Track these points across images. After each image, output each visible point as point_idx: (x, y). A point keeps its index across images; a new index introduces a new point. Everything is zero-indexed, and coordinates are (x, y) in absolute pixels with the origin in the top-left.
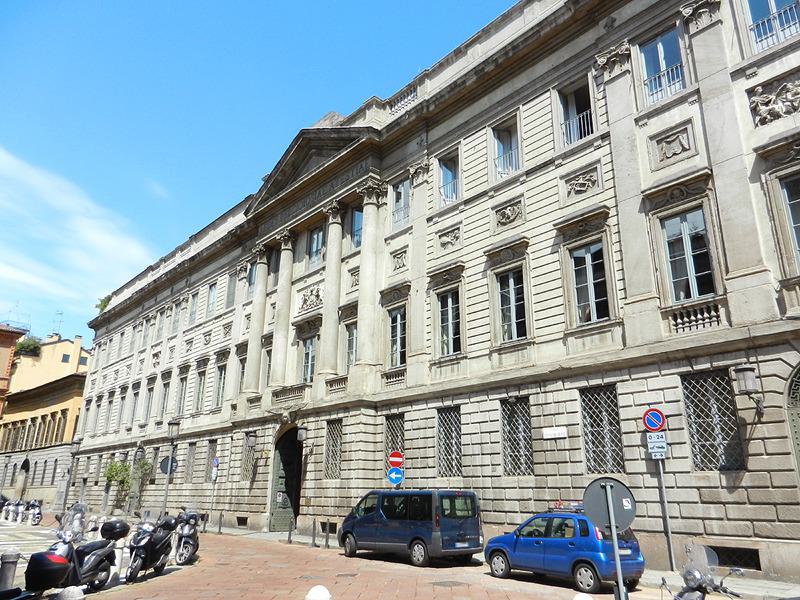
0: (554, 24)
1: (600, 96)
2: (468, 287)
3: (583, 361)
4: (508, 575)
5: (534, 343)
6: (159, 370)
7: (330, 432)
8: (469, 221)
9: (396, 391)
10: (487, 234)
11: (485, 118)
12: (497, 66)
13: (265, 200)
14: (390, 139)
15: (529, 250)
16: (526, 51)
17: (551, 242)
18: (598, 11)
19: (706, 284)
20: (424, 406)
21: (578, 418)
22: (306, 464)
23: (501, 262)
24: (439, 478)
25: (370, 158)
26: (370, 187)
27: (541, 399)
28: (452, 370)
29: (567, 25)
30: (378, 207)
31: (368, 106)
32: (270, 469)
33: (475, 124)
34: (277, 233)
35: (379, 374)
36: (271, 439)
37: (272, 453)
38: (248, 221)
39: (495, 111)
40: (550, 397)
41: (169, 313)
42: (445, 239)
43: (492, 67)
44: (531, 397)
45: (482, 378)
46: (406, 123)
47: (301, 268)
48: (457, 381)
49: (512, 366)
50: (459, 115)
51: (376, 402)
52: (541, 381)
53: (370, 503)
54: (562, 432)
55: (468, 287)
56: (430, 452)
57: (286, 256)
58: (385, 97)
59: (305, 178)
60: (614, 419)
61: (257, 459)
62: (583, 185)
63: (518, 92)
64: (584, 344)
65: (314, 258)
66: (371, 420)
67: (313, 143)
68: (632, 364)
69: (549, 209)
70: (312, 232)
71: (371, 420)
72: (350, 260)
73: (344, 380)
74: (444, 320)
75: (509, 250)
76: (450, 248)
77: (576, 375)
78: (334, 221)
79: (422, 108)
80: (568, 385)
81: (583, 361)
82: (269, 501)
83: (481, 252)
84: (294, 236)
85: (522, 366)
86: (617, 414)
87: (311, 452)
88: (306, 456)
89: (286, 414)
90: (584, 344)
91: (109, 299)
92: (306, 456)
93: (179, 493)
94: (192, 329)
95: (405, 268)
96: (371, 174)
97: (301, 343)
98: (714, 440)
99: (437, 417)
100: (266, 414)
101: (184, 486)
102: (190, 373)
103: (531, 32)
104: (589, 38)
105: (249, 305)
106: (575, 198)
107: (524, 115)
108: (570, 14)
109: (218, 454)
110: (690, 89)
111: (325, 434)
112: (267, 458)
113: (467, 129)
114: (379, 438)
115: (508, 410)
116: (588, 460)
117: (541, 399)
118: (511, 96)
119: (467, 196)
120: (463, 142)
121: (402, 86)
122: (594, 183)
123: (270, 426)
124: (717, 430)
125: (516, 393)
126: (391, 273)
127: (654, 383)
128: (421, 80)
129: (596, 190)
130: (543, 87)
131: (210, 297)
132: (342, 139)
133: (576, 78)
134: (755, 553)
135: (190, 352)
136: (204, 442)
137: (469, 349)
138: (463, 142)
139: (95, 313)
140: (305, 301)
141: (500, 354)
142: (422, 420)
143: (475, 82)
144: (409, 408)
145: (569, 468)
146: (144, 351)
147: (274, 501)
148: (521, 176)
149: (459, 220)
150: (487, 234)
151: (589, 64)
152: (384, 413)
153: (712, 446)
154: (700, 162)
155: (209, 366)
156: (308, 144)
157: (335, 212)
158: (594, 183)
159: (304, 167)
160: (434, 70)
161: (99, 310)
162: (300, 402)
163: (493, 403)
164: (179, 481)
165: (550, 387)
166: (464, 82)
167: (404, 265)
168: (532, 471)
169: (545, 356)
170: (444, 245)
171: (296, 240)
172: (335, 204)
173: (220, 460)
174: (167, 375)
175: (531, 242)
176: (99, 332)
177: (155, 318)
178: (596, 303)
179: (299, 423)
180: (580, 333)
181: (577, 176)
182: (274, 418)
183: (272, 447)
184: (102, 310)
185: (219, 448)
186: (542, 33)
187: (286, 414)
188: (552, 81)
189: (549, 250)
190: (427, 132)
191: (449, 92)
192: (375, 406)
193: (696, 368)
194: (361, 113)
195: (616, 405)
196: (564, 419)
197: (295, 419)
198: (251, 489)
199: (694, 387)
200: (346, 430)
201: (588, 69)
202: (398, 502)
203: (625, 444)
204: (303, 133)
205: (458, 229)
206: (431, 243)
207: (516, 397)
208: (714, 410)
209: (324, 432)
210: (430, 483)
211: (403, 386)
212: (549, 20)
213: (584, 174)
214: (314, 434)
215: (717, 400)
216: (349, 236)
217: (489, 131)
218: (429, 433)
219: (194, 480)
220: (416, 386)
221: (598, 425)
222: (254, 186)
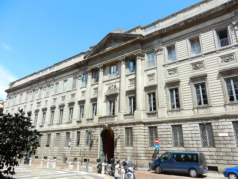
0: (216, 11)
1: (233, 33)
2: (182, 88)
3: (234, 113)
4: (160, 173)
5: (212, 106)
6: (40, 108)
7: (126, 132)
8: (207, 60)
9: (153, 119)
10: (189, 72)
11: (187, 35)
12: (193, 21)
13: (92, 55)
14: (147, 39)
15: (207, 78)
16: (203, 17)
17: (188, 82)
18: (232, 8)
19: (155, 109)
20: (166, 124)
21: (232, 130)
22: (116, 142)
23: (196, 81)
24: (174, 148)
25: (139, 44)
26: (140, 54)
27: (217, 124)
28: (177, 113)
29: (220, 11)
30: (142, 60)
31: (137, 28)
32: (99, 143)
33: (182, 37)
34: (98, 65)
35: (145, 114)
36: (99, 133)
37: (100, 138)
38: (84, 61)
39: (190, 34)
40: (220, 124)
41: (45, 89)
42: (170, 72)
43: (191, 21)
44: (158, 127)
45: (192, 116)
46: (155, 35)
47: (107, 77)
48: (180, 117)
49: (176, 116)
50: (176, 34)
51: (145, 122)
52: (217, 118)
53: (167, 156)
54: (227, 135)
55: (182, 88)
56: (170, 139)
57: (101, 73)
58: (142, 26)
59: (108, 49)
60: (156, 134)
61: (93, 139)
62: (228, 60)
63: (200, 29)
64: (233, 108)
65: (112, 74)
66: (143, 128)
67: (113, 38)
68: (187, 120)
69: (187, 72)
70: (111, 66)
71: (143, 128)
72: (129, 76)
73: (43, 126)
74: (110, 108)
75: (200, 77)
76: (173, 75)
77: (230, 117)
78: (124, 63)
79: (162, 31)
80: (227, 120)
81: (234, 113)
82: (99, 154)
83: (218, 71)
84: (104, 67)
85: (208, 113)
86: (157, 133)
87: (119, 138)
88: (116, 139)
89: (107, 125)
90: (233, 108)
91: (14, 82)
92: (116, 139)
93: (52, 150)
94: (14, 106)
95: (154, 80)
96: (140, 49)
97: (108, 102)
98: (178, 140)
99: (148, 129)
100: (97, 125)
101: (55, 148)
102: (56, 109)
103: (208, 12)
104: (228, 16)
105: (83, 88)
106: (224, 63)
107: (177, 45)
108: (223, 8)
109: (71, 137)
110: (156, 67)
111: (124, 132)
112: (98, 139)
113: (179, 39)
114: (146, 134)
115: (202, 127)
116: (125, 144)
117: (217, 124)
118: (197, 30)
119: (205, 52)
120: (177, 43)
121: (150, 23)
122: (232, 59)
123: (98, 128)
124: (208, 137)
125: (206, 122)
126: (147, 81)
127: (192, 125)
128: (158, 22)
129: (233, 61)
130: (210, 29)
131: (65, 85)
132: (127, 37)
133: (222, 28)
134: (217, 167)
135: (55, 103)
136: (64, 134)
137: (212, 103)
138: (177, 43)
139: (8, 88)
140: (109, 88)
141: (197, 109)
142: (165, 130)
143: (183, 25)
144: (159, 125)
145: (230, 146)
146: (33, 101)
147: (100, 154)
148: (203, 55)
149: (177, 67)
150: (189, 72)
151: (228, 24)
152: (148, 126)
153: (177, 142)
154: (155, 83)
155: (65, 108)
156: (111, 38)
157: (124, 60)
158: (232, 59)
159: (108, 45)
160: (163, 20)
161: (10, 86)
162: (113, 121)
163: (196, 125)
164: (52, 146)
165: (220, 121)
166: (179, 24)
167: (153, 79)
168: (132, 146)
169: (187, 113)
170: (170, 74)
171: (104, 68)
172: (102, 65)
173: (72, 139)
174: (44, 110)
175: (208, 75)
176: (10, 94)
177: (38, 90)
178: (176, 104)
179: (112, 128)
180: (172, 111)
181: (225, 57)
182: (100, 126)
183: (99, 136)
184: (11, 86)
185: (71, 135)
186: (211, 13)
187: (107, 125)
188: (214, 27)
189: (216, 78)
190: (161, 38)
191: (173, 27)
192: (144, 124)
193: (128, 126)
194: (134, 30)
195: (157, 131)
196: (227, 131)
197: (110, 127)
198: (90, 149)
199: (174, 128)
200: (51, 136)
201: (228, 25)
202: (182, 156)
203: (184, 140)
204: (110, 34)
205: (176, 69)
206: (165, 73)
207: (206, 123)
208: (154, 135)
209: (124, 131)
210: (170, 149)
211: (42, 129)
212: (215, 9)
213: (228, 56)
214: (120, 133)
215: (179, 132)
216: (128, 69)
217: (188, 40)
218: (169, 133)
219: (59, 146)
220: (163, 118)
221: (152, 136)
222: (87, 49)
